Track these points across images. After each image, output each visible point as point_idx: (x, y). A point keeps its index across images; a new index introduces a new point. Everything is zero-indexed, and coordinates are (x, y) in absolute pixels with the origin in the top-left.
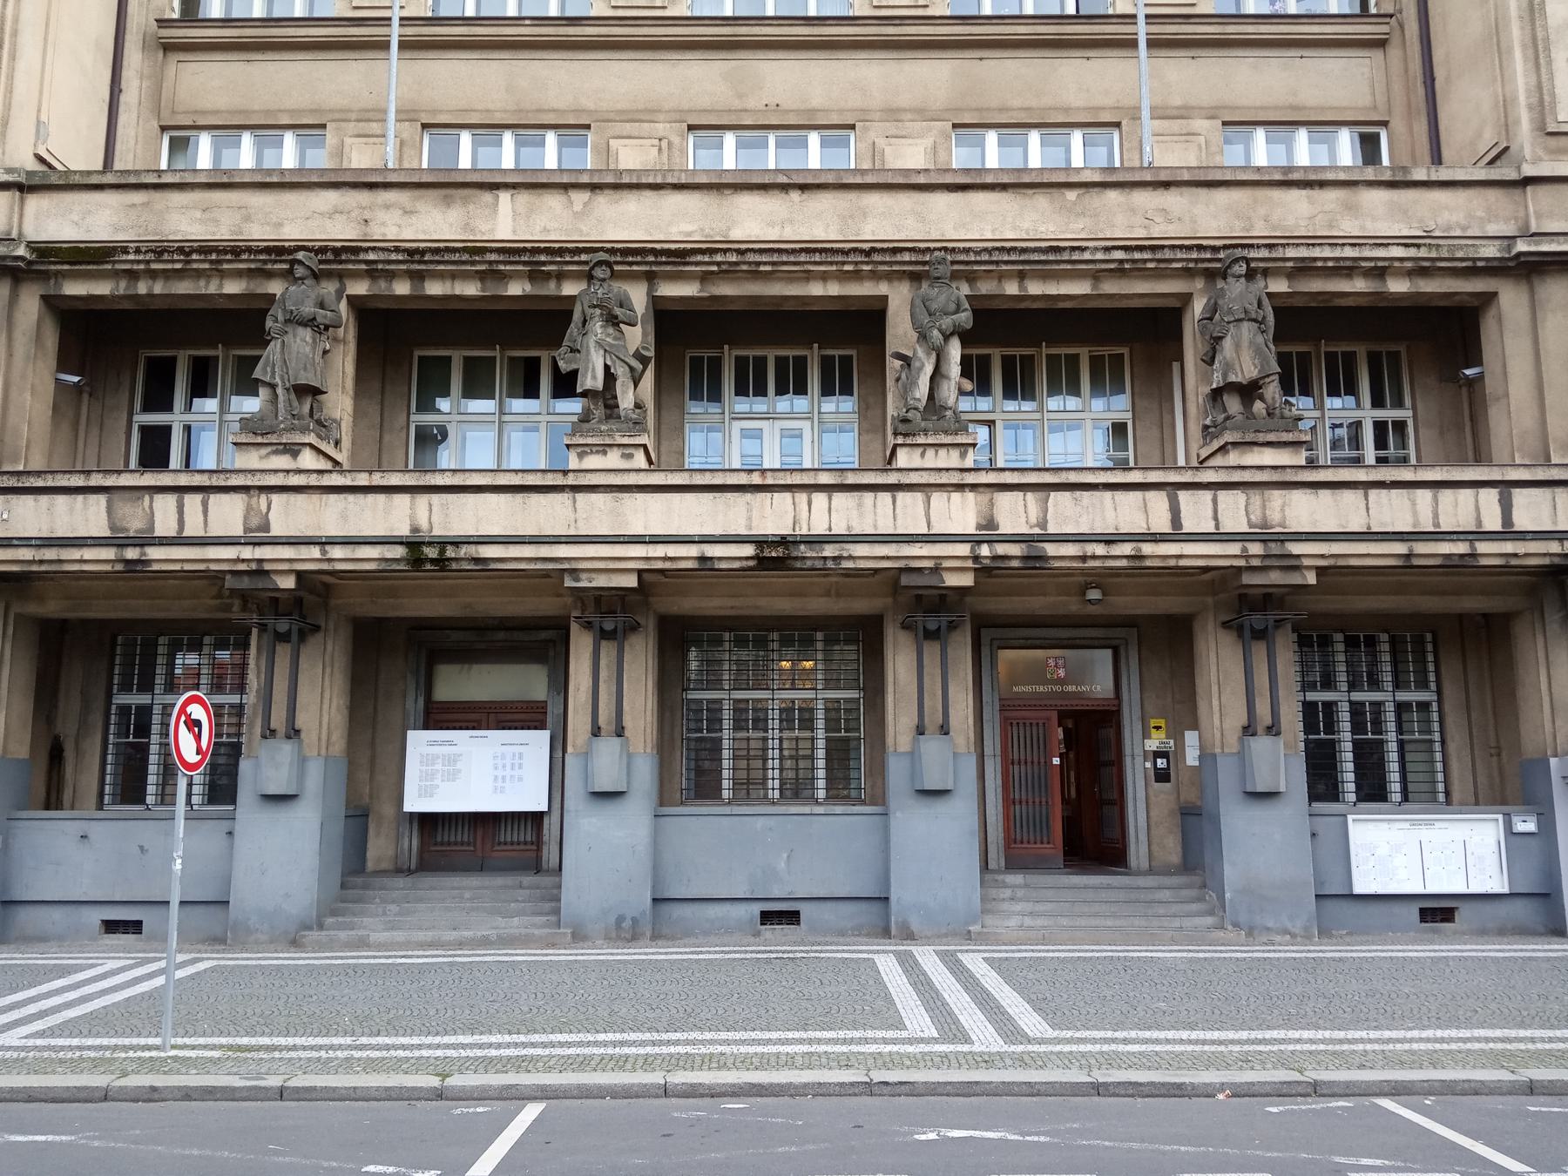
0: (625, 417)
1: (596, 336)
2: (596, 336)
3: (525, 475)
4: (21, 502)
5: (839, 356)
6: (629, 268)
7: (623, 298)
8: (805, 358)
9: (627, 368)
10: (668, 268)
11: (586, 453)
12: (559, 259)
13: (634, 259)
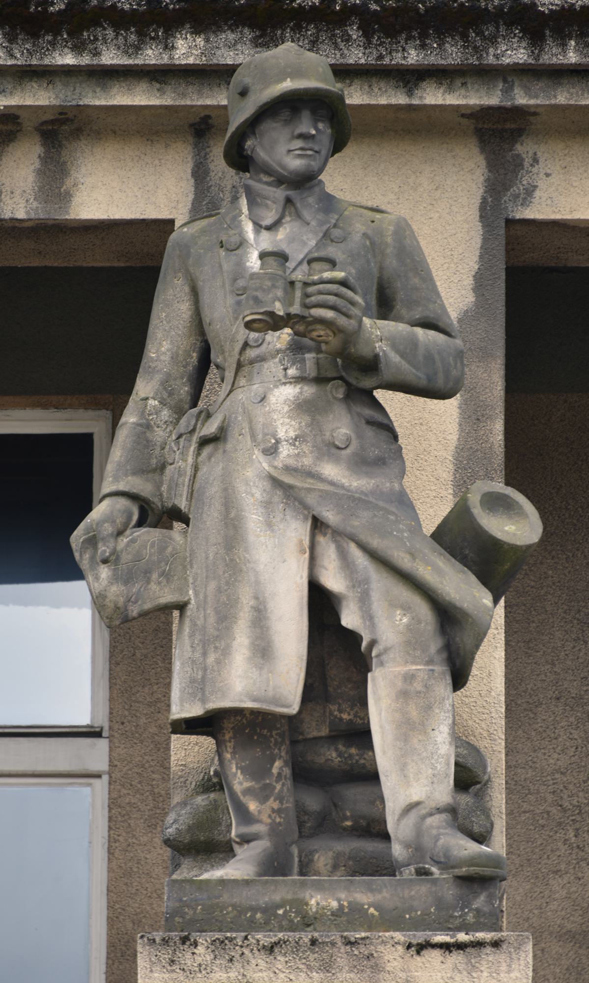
0: (417, 848)
1: (271, 451)
2: (271, 451)
4: (478, 587)
6: (400, 99)
7: (392, 263)
8: (84, 443)
9: (424, 610)
12: (69, 59)
13: (433, 59)
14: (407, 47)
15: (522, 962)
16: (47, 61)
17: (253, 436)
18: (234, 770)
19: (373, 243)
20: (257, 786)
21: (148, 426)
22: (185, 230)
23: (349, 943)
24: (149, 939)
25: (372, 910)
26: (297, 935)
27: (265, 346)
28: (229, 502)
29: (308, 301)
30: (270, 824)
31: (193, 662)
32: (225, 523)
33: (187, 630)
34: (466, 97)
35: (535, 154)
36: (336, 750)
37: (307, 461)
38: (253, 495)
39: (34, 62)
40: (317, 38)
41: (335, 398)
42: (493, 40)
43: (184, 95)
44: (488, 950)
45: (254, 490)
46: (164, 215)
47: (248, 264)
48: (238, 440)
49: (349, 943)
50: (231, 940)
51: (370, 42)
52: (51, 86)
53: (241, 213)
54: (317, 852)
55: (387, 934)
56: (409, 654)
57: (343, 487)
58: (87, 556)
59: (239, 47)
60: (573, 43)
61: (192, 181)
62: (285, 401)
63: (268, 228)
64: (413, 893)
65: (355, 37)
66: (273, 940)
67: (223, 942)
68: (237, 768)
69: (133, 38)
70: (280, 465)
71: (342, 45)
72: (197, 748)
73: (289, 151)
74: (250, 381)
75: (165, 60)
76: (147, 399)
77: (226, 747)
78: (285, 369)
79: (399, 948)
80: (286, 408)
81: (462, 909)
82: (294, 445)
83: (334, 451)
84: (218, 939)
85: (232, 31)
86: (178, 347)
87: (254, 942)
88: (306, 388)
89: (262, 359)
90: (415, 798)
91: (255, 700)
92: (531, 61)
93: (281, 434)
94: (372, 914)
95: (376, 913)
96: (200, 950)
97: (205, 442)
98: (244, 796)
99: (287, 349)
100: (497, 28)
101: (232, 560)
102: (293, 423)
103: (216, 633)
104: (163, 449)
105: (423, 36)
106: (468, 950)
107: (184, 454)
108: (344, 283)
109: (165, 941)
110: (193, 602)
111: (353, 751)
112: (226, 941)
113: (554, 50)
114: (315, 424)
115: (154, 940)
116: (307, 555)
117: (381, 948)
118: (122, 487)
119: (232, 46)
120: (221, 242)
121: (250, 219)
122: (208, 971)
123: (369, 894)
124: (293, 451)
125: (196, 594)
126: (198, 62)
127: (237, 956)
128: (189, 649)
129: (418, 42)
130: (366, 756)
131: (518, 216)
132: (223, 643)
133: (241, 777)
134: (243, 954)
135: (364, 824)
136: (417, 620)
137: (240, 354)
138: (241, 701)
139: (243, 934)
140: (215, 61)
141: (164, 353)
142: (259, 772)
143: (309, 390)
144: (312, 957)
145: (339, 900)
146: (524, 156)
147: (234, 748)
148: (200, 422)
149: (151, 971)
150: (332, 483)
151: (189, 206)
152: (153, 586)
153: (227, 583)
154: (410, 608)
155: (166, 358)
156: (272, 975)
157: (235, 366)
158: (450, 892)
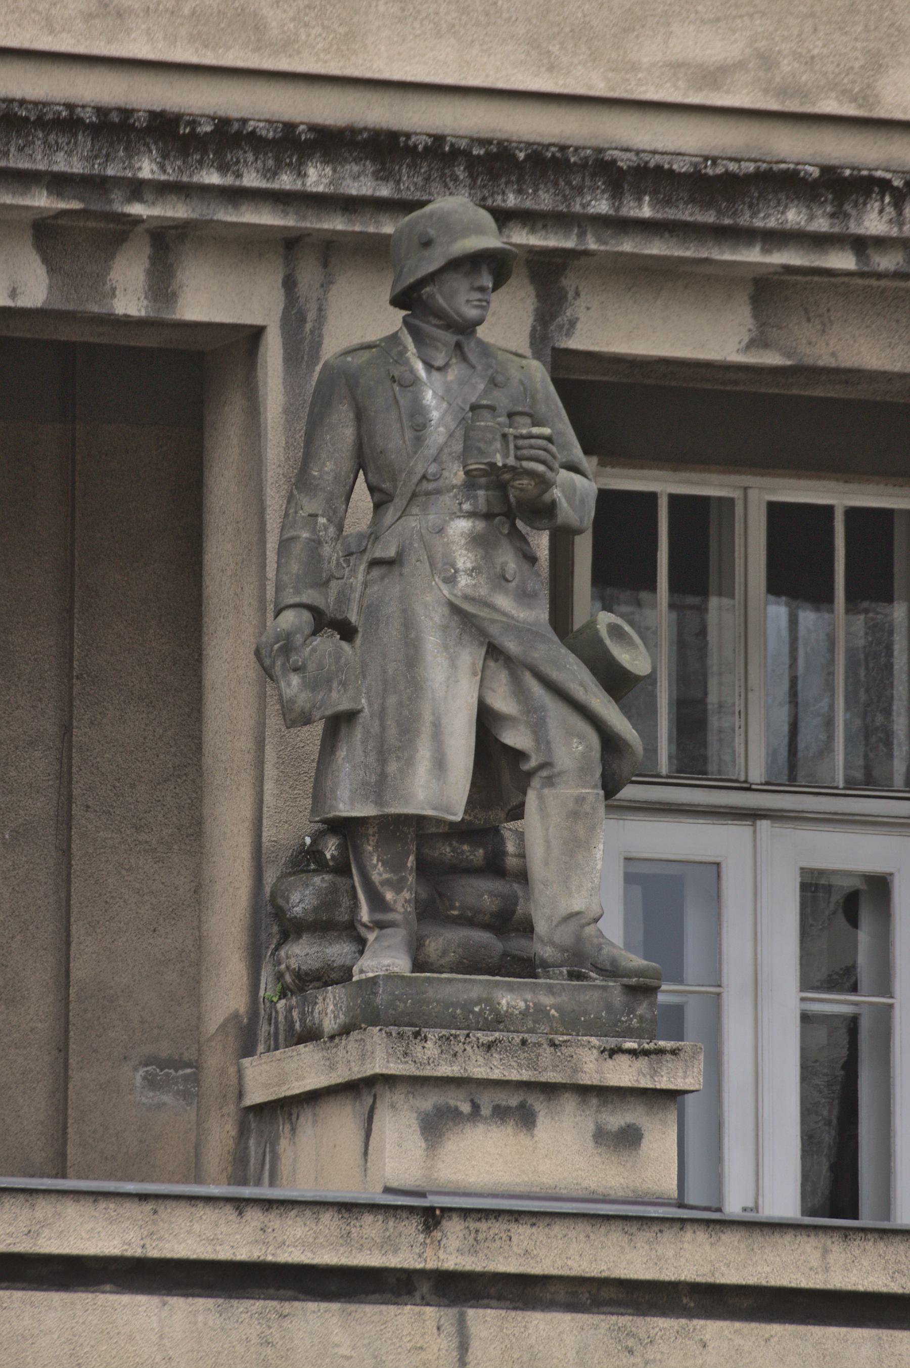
1: (451, 580)
3: (274, 1220)
5: (852, 514)
10: (656, 248)
11: (455, 1115)
14: (507, 191)
15: (695, 1070)
16: (195, 179)
17: (432, 565)
18: (375, 861)
19: (525, 389)
20: (395, 878)
21: (319, 542)
22: (349, 359)
23: (553, 1044)
24: (386, 1033)
25: (553, 1012)
26: (511, 1035)
27: (442, 480)
28: (408, 624)
29: (519, 453)
30: (404, 913)
31: (366, 766)
32: (406, 642)
33: (359, 736)
34: (546, 239)
35: (577, 288)
36: (450, 845)
37: (483, 591)
38: (431, 619)
39: (185, 179)
40: (430, 176)
41: (501, 533)
42: (580, 191)
43: (304, 218)
44: (669, 1057)
45: (433, 615)
46: (257, 321)
47: (424, 402)
48: (415, 566)
49: (553, 1044)
50: (456, 1037)
51: (475, 183)
52: (188, 200)
53: (406, 349)
54: (428, 937)
55: (585, 1038)
56: (581, 779)
57: (512, 617)
58: (279, 663)
59: (362, 178)
60: (647, 198)
61: (282, 291)
62: (462, 534)
63: (439, 369)
64: (587, 998)
65: (461, 177)
66: (491, 1039)
67: (448, 1038)
68: (378, 861)
69: (271, 163)
70: (460, 594)
71: (451, 184)
72: (286, 825)
73: (468, 301)
74: (425, 509)
75: (298, 186)
76: (316, 516)
77: (368, 840)
78: (460, 504)
79: (595, 1051)
80: (463, 542)
81: (628, 1015)
82: (471, 576)
83: (504, 583)
84: (445, 1035)
85: (356, 163)
86: (341, 468)
87: (475, 1039)
88: (477, 522)
89: (438, 492)
90: (577, 908)
91: (435, 809)
92: (611, 212)
93: (460, 565)
94: (553, 1016)
95: (556, 1014)
96: (429, 1044)
97: (375, 563)
98: (382, 886)
99: (462, 485)
100: (583, 179)
101: (413, 678)
102: (470, 555)
103: (398, 744)
104: (329, 563)
105: (520, 180)
106: (652, 1056)
107: (354, 571)
108: (549, 439)
109: (401, 1035)
110: (366, 710)
111: (466, 847)
112: (452, 1038)
113: (632, 204)
114: (487, 557)
115: (391, 1034)
116: (479, 677)
117: (579, 1051)
118: (304, 599)
119: (356, 178)
120: (393, 377)
121: (419, 357)
122: (436, 1063)
123: (551, 997)
124: (470, 581)
125: (370, 704)
126: (327, 190)
127: (460, 1052)
128: (361, 754)
129: (515, 187)
130: (476, 853)
131: (563, 345)
132: (406, 754)
133: (381, 869)
134: (465, 1050)
135: (470, 914)
136: (589, 748)
137: (417, 485)
138: (423, 809)
139: (466, 1032)
140: (342, 191)
141: (328, 473)
142: (395, 865)
143: (480, 525)
144: (522, 1056)
145: (526, 1001)
146: (568, 289)
147: (377, 842)
148: (370, 543)
149: (388, 1062)
150: (504, 614)
151: (280, 315)
152: (334, 694)
153: (410, 699)
154: (584, 737)
155: (330, 478)
156: (489, 1070)
157: (409, 495)
158: (617, 997)
